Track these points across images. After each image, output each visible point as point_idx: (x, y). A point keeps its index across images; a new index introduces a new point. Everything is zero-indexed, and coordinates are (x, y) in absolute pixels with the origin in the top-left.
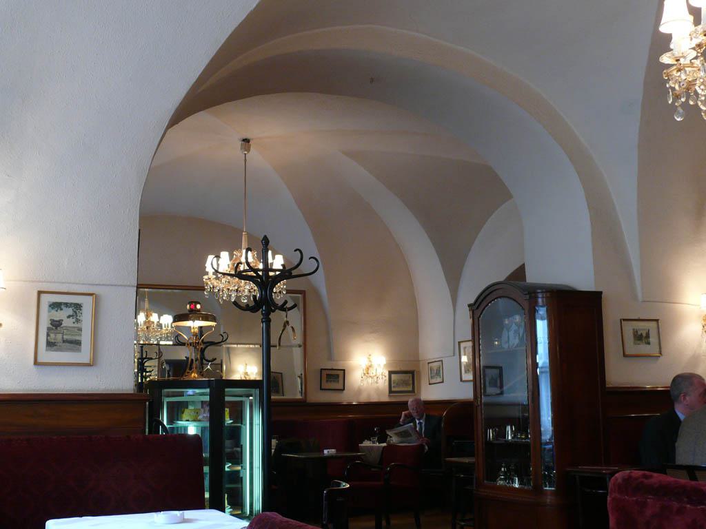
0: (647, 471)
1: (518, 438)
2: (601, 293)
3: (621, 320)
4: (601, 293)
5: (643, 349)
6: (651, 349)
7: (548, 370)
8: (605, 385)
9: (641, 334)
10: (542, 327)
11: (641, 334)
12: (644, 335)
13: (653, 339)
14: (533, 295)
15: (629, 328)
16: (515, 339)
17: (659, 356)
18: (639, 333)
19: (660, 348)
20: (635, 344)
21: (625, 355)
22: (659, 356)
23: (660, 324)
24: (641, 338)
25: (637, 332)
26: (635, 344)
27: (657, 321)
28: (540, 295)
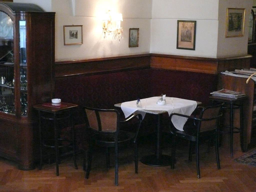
0: (238, 59)
1: (95, 133)
2: (55, 13)
3: (64, 26)
4: (55, 13)
5: (74, 40)
6: (78, 40)
7: (20, 28)
8: (54, 60)
9: (73, 33)
10: (23, 23)
11: (73, 33)
12: (75, 33)
13: (79, 35)
14: (18, 13)
15: (68, 30)
16: (6, 31)
17: (81, 44)
18: (72, 33)
19: (82, 40)
20: (70, 38)
21: (65, 44)
22: (81, 44)
23: (83, 28)
24: (74, 35)
25: (71, 32)
26: (70, 38)
27: (82, 26)
28: (22, 14)
